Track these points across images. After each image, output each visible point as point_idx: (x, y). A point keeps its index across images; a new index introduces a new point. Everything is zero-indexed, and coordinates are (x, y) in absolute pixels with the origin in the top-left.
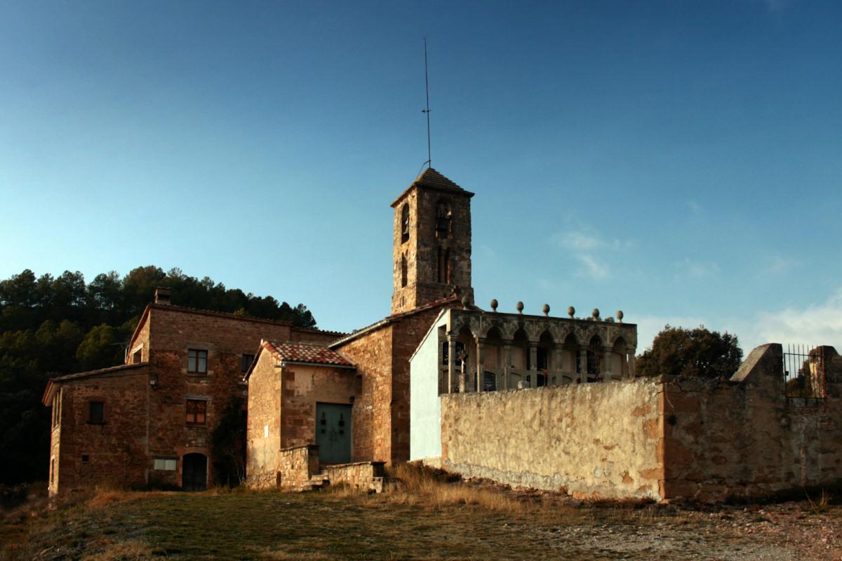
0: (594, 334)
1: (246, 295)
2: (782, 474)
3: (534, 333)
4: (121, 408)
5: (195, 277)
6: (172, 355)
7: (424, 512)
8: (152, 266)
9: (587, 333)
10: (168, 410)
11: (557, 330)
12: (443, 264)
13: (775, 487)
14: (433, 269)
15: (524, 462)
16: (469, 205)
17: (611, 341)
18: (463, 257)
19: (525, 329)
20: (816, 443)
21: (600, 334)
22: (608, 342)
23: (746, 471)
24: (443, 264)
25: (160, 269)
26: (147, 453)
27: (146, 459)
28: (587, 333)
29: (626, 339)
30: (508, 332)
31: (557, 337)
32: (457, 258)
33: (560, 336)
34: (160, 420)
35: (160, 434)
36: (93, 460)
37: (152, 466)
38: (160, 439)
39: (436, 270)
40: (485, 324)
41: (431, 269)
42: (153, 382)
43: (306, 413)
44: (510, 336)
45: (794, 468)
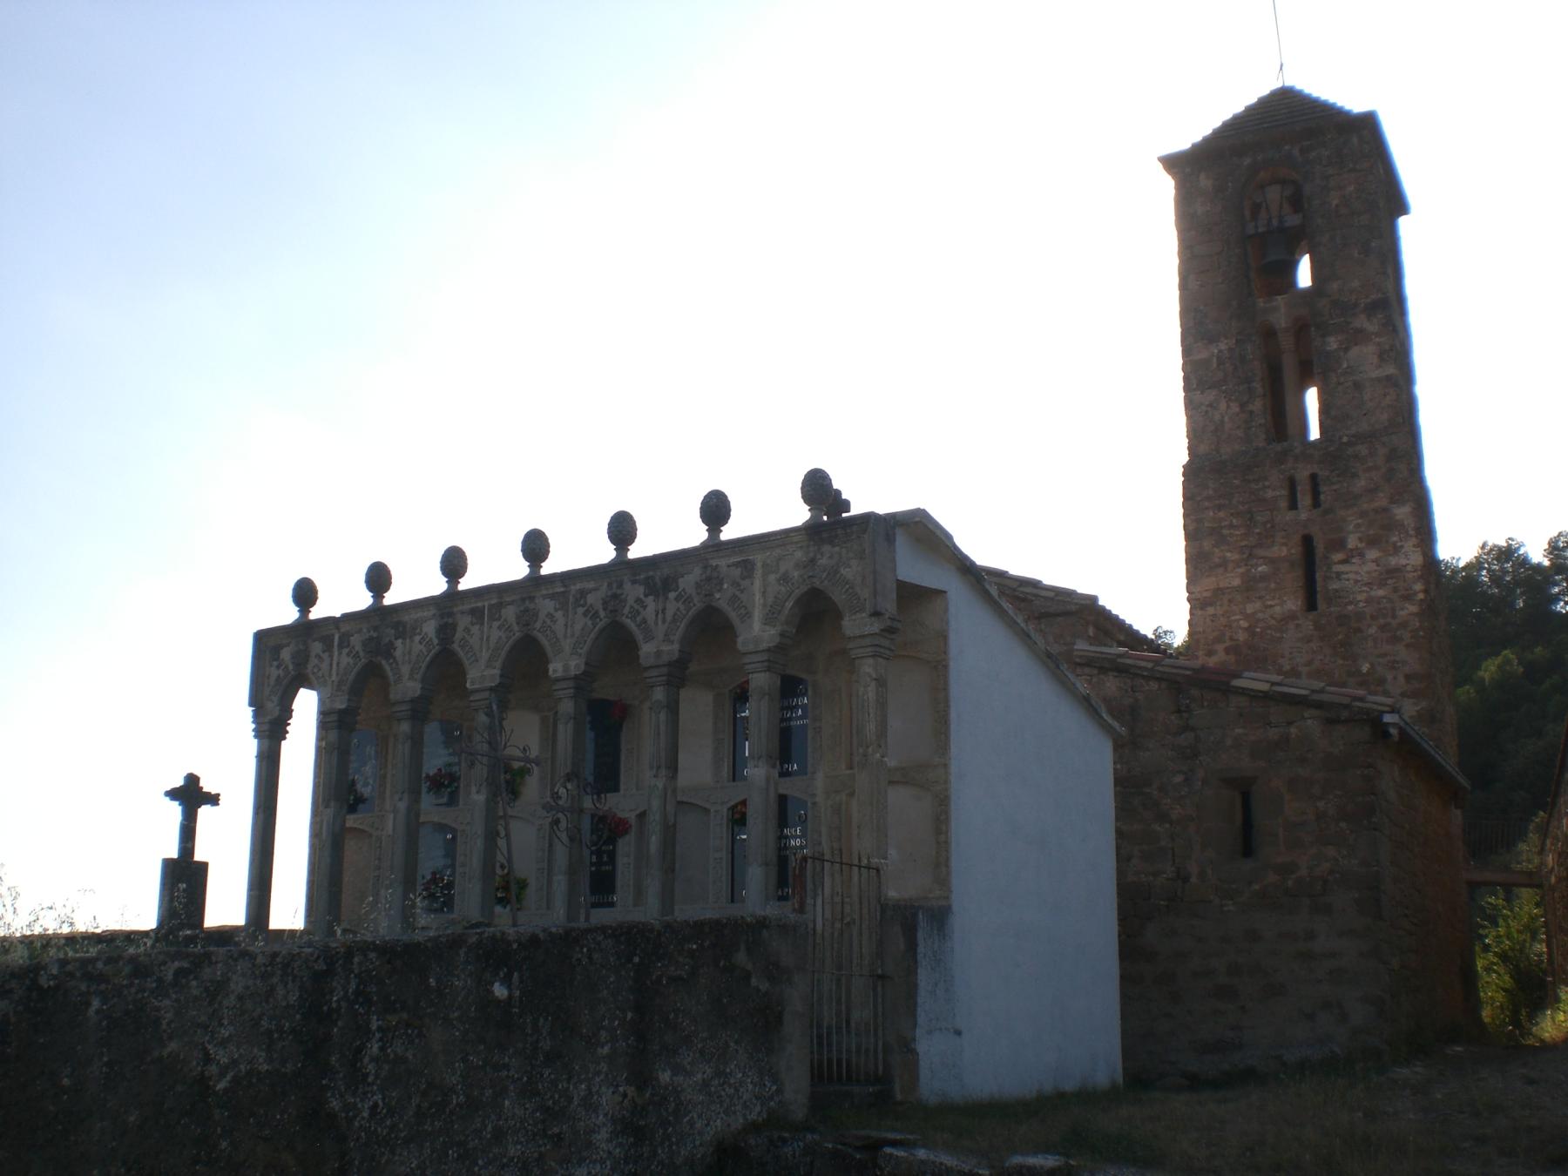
0: (698, 604)
1: (1151, 636)
3: (485, 655)
8: (1183, 467)
9: (672, 608)
11: (559, 627)
14: (1242, 406)
15: (421, 905)
16: (1119, 895)
17: (769, 620)
18: (1360, 331)
19: (456, 647)
21: (721, 600)
22: (757, 625)
25: (253, 730)
28: (672, 608)
29: (838, 596)
30: (405, 670)
31: (649, 637)
33: (567, 645)
40: (345, 660)
41: (1235, 408)
44: (411, 684)
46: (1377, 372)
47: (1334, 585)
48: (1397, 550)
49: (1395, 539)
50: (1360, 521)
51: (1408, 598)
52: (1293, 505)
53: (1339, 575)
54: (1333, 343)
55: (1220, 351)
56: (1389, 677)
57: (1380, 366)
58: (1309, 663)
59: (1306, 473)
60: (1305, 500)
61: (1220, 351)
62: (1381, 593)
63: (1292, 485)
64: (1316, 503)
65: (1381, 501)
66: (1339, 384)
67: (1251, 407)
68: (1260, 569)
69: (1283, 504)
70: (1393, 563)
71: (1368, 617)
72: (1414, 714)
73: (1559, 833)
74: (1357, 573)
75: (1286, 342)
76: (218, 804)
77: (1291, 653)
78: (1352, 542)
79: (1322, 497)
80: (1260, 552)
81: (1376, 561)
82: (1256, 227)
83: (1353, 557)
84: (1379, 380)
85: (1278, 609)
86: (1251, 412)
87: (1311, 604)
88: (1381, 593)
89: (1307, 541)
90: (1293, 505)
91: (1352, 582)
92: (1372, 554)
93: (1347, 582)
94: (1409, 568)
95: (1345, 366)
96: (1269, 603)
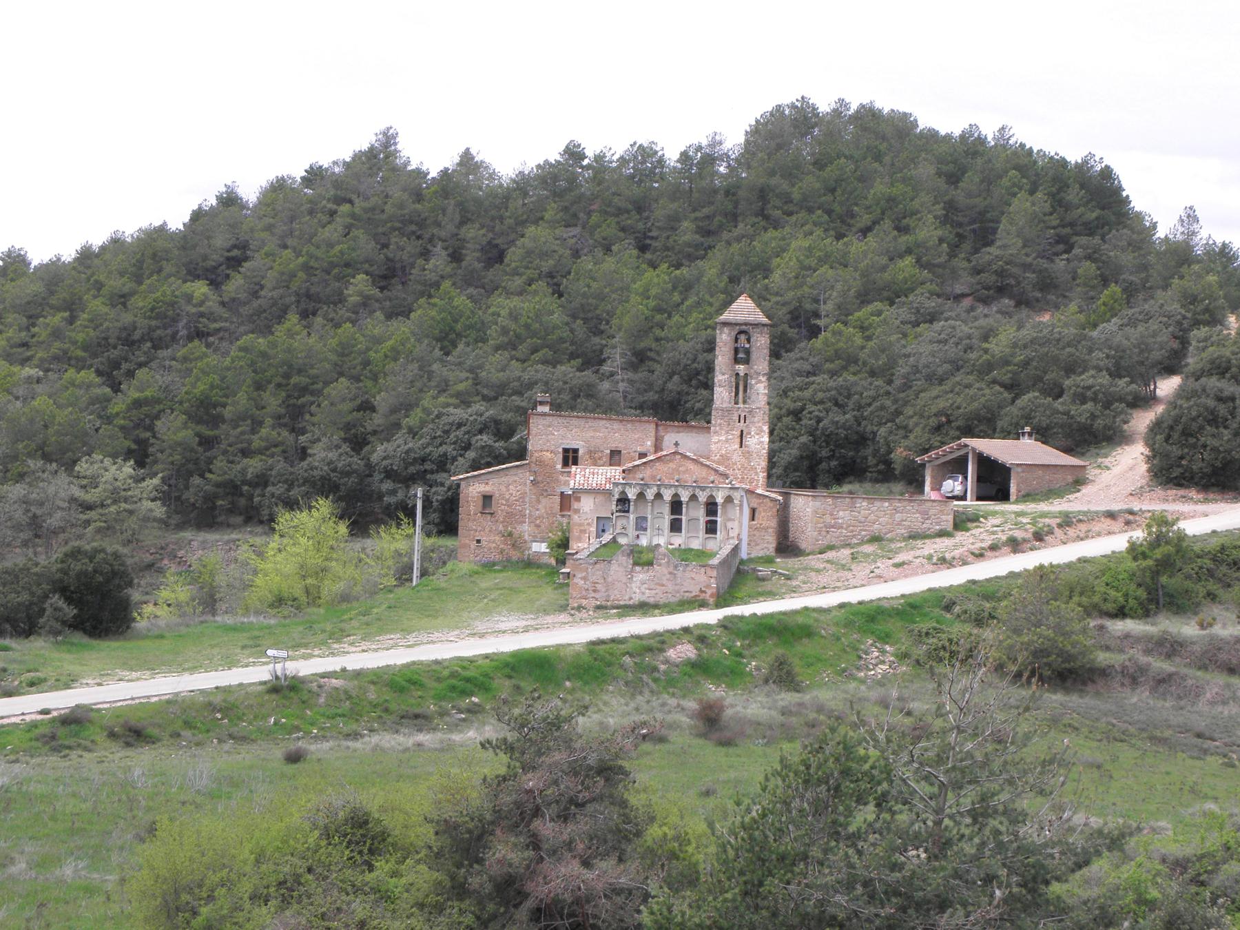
2: (627, 598)
4: (507, 500)
5: (914, 114)
6: (548, 454)
7: (910, 527)
10: (544, 501)
12: (741, 388)
13: (622, 603)
20: (646, 586)
23: (609, 596)
24: (741, 388)
26: (526, 537)
27: (526, 542)
32: (753, 382)
34: (538, 510)
35: (538, 522)
36: (484, 543)
37: (530, 548)
38: (538, 526)
39: (733, 394)
42: (532, 478)
43: (588, 524)
45: (633, 596)
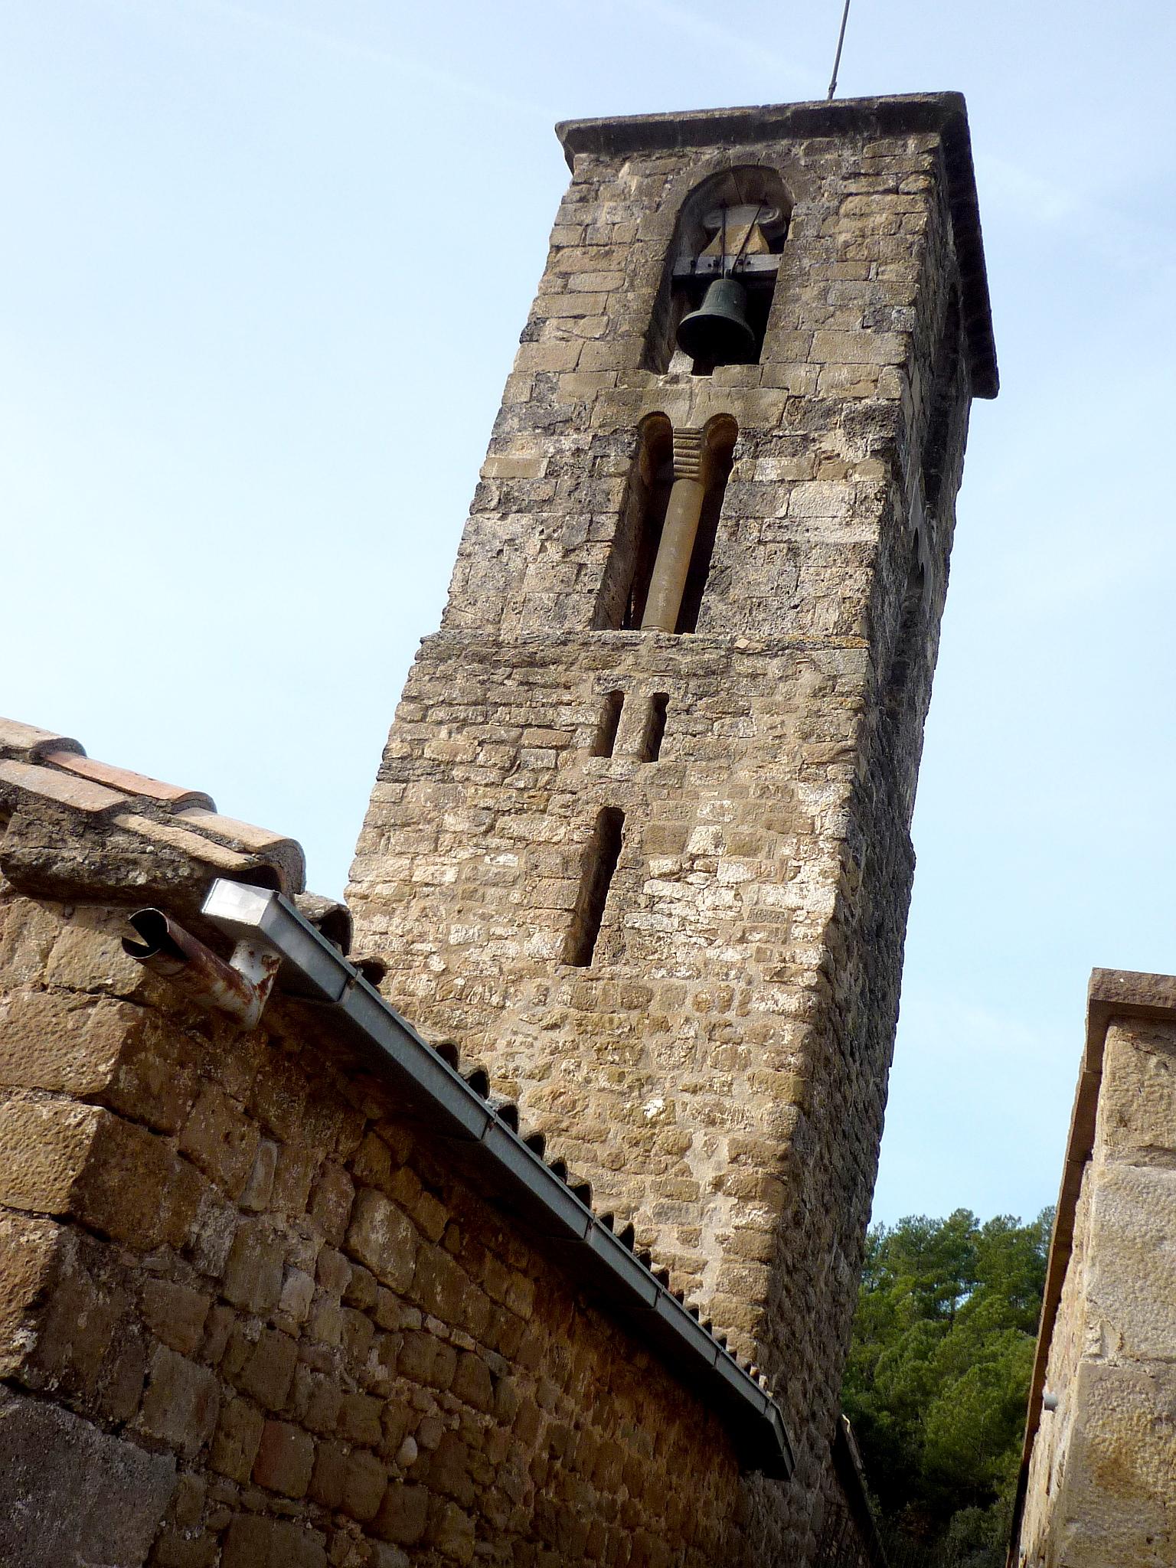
41: (554, 552)
46: (840, 534)
47: (637, 919)
48: (786, 874)
49: (787, 851)
50: (726, 803)
51: (780, 977)
52: (604, 746)
53: (653, 901)
54: (770, 468)
55: (560, 451)
56: (699, 1140)
57: (848, 524)
58: (544, 1073)
59: (647, 692)
60: (629, 739)
61: (560, 451)
62: (732, 955)
63: (615, 700)
64: (650, 751)
65: (779, 771)
66: (760, 542)
67: (582, 557)
68: (502, 859)
69: (585, 739)
70: (770, 900)
71: (689, 1001)
72: (730, 1231)
73: (639, 778)
74: (690, 903)
75: (686, 460)
76: (560, 128)
77: (509, 1044)
78: (699, 840)
79: (665, 743)
80: (514, 825)
81: (736, 888)
82: (694, 264)
83: (692, 870)
84: (839, 548)
85: (512, 948)
86: (581, 566)
87: (582, 955)
88: (732, 955)
89: (611, 823)
90: (604, 746)
91: (676, 921)
92: (731, 871)
93: (665, 920)
94: (801, 915)
95: (782, 513)
96: (499, 931)
